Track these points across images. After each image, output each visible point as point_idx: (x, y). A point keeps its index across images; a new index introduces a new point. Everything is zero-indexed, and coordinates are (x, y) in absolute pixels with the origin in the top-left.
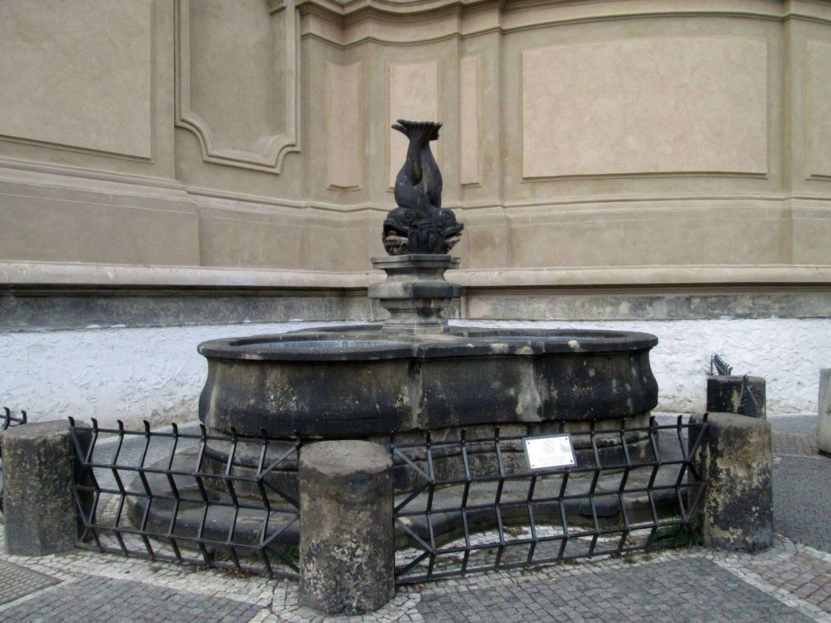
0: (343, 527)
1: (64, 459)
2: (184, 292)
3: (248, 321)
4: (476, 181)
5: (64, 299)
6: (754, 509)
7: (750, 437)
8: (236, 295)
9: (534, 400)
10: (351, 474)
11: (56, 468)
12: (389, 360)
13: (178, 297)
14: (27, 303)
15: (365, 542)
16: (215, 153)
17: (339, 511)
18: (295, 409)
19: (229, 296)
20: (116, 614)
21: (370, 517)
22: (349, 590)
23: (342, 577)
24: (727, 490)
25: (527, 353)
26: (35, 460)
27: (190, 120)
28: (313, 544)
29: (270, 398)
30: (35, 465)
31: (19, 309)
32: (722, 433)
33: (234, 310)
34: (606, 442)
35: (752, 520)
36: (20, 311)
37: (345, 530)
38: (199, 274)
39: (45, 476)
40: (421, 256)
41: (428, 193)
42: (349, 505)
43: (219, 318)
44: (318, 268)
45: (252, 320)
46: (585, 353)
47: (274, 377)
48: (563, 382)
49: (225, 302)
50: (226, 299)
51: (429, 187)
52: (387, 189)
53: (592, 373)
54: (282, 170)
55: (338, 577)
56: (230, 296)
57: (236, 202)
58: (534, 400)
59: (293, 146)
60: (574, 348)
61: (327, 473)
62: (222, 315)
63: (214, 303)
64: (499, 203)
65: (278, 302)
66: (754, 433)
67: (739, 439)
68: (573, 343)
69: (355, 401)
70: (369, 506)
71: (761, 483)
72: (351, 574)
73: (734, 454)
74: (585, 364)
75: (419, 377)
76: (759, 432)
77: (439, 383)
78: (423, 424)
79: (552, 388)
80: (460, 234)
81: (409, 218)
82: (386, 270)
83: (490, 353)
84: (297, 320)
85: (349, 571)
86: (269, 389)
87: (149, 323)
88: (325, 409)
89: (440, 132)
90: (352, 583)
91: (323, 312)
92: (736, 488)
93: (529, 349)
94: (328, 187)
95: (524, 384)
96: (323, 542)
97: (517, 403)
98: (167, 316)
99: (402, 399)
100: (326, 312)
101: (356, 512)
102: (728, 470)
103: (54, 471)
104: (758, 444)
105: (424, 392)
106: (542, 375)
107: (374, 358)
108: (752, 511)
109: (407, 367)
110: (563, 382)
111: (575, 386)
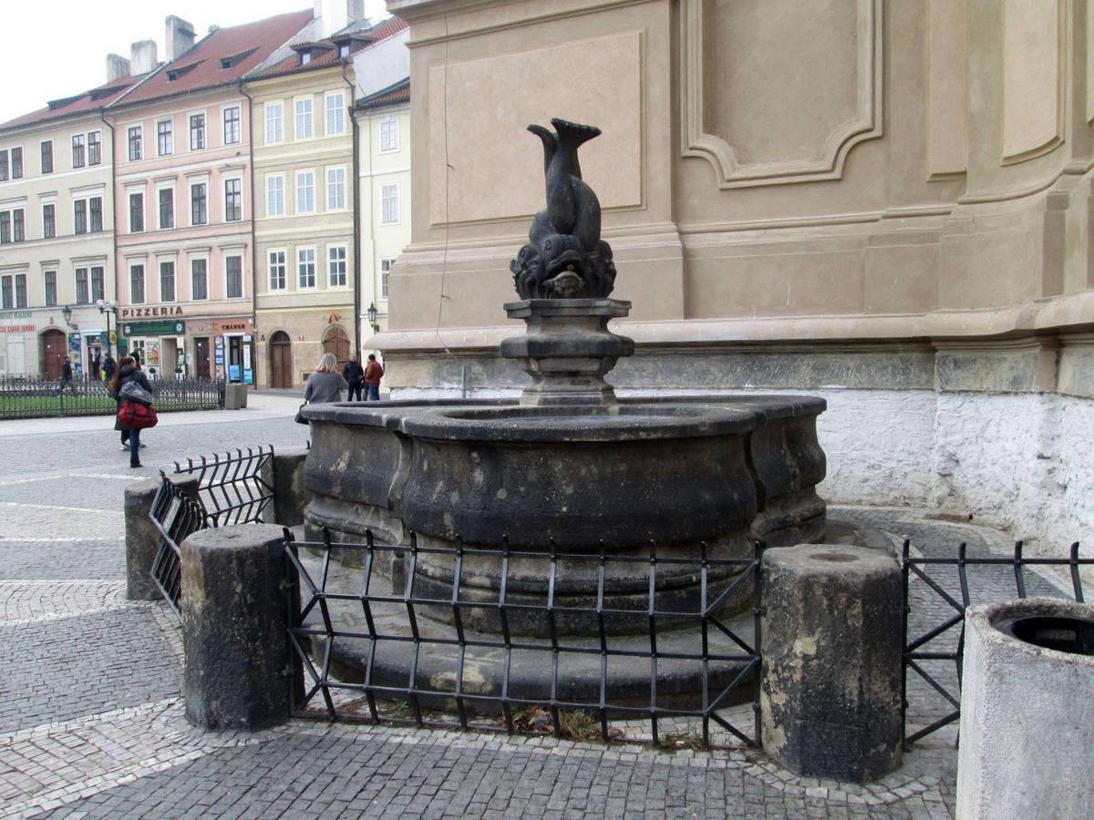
2: (660, 351)
3: (750, 386)
5: (834, 355)
8: (733, 353)
13: (655, 356)
14: (513, 363)
19: (724, 354)
20: (734, 761)
27: (699, 145)
31: (508, 369)
33: (730, 371)
34: (426, 571)
36: (508, 371)
38: (654, 330)
43: (707, 381)
44: (880, 310)
45: (756, 384)
49: (717, 360)
50: (719, 357)
52: (1001, 162)
54: (647, 206)
56: (727, 353)
57: (763, 231)
62: (712, 377)
63: (702, 363)
65: (802, 361)
84: (833, 386)
87: (621, 383)
91: (889, 377)
94: (928, 178)
98: (642, 377)
100: (894, 375)
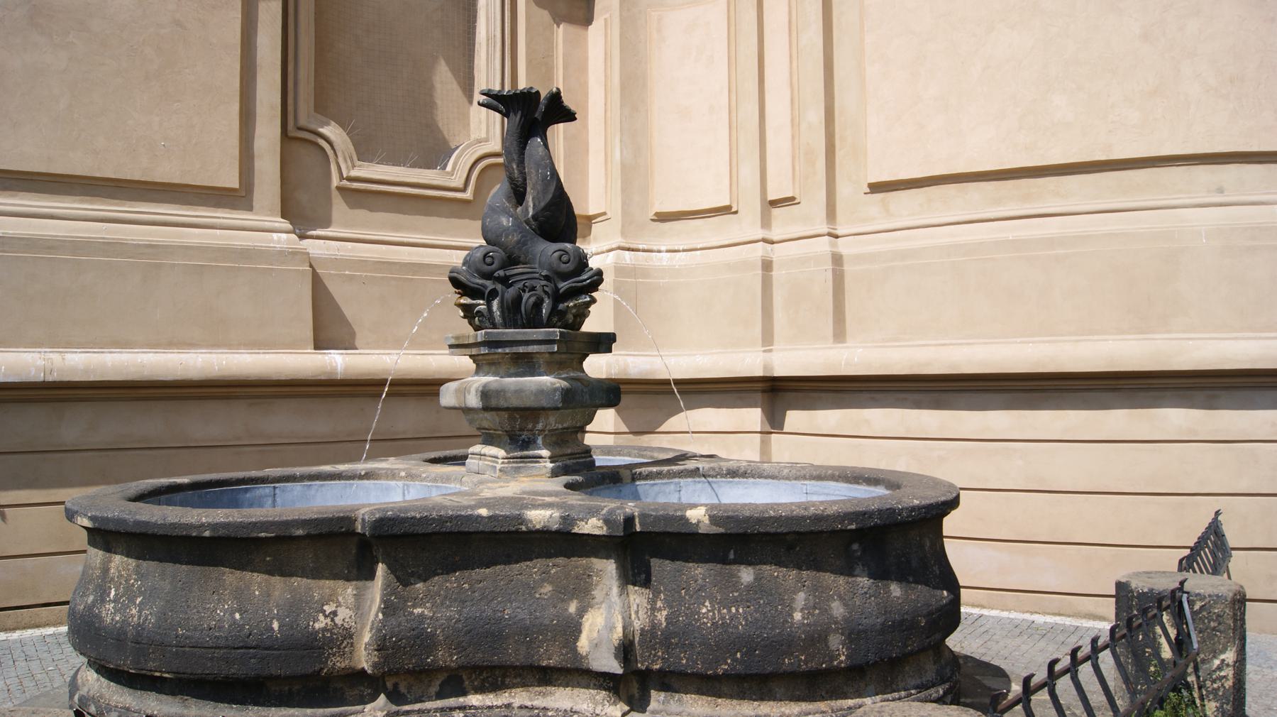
4: (789, 195)
12: (299, 537)
16: (354, 173)
18: (135, 619)
25: (597, 532)
40: (504, 333)
64: (760, 234)
69: (232, 614)
79: (659, 604)
81: (492, 264)
88: (179, 625)
93: (600, 523)
95: (598, 593)
97: (580, 632)
111: (707, 604)
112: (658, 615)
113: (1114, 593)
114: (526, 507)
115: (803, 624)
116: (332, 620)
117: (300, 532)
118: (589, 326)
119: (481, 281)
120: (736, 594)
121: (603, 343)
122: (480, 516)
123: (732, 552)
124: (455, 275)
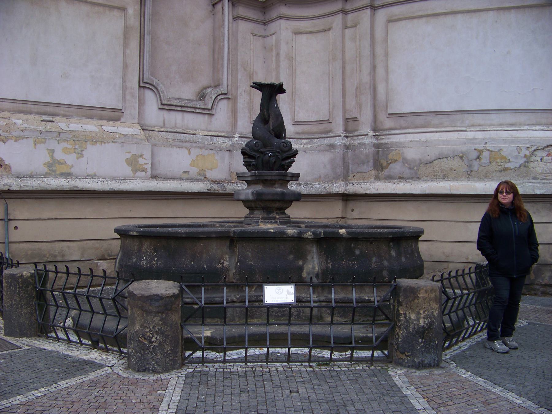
0: (145, 325)
1: (32, 286)
6: (420, 340)
7: (419, 293)
9: (314, 268)
10: (150, 295)
11: (27, 291)
12: (214, 237)
15: (157, 333)
17: (143, 316)
18: (156, 265)
21: (160, 320)
22: (148, 360)
23: (144, 352)
24: (404, 328)
26: (17, 285)
28: (132, 333)
29: (143, 258)
30: (16, 288)
32: (402, 290)
35: (419, 347)
37: (146, 326)
39: (21, 294)
41: (273, 130)
42: (148, 312)
46: (350, 238)
47: (147, 245)
48: (337, 257)
51: (273, 126)
53: (357, 252)
55: (142, 352)
58: (314, 268)
59: (225, 94)
60: (342, 235)
61: (137, 294)
66: (422, 291)
67: (412, 295)
68: (342, 231)
70: (160, 314)
71: (427, 324)
72: (149, 351)
73: (409, 304)
74: (353, 245)
75: (236, 250)
76: (425, 290)
77: (250, 254)
78: (236, 279)
79: (329, 261)
80: (296, 157)
82: (246, 181)
83: (285, 236)
85: (148, 349)
86: (144, 253)
89: (284, 87)
90: (149, 356)
92: (409, 327)
93: (311, 234)
95: (309, 257)
96: (135, 332)
97: (303, 270)
99: (223, 263)
101: (152, 317)
102: (405, 314)
103: (26, 293)
104: (425, 299)
105: (238, 259)
106: (323, 252)
107: (202, 236)
108: (419, 342)
109: (228, 243)
110: (337, 257)
112: (329, 264)
113: (476, 241)
114: (285, 229)
115: (375, 267)
116: (223, 265)
117: (214, 236)
118: (291, 170)
119: (254, 153)
120: (354, 258)
121: (296, 176)
122: (271, 232)
123: (353, 244)
124: (244, 150)
